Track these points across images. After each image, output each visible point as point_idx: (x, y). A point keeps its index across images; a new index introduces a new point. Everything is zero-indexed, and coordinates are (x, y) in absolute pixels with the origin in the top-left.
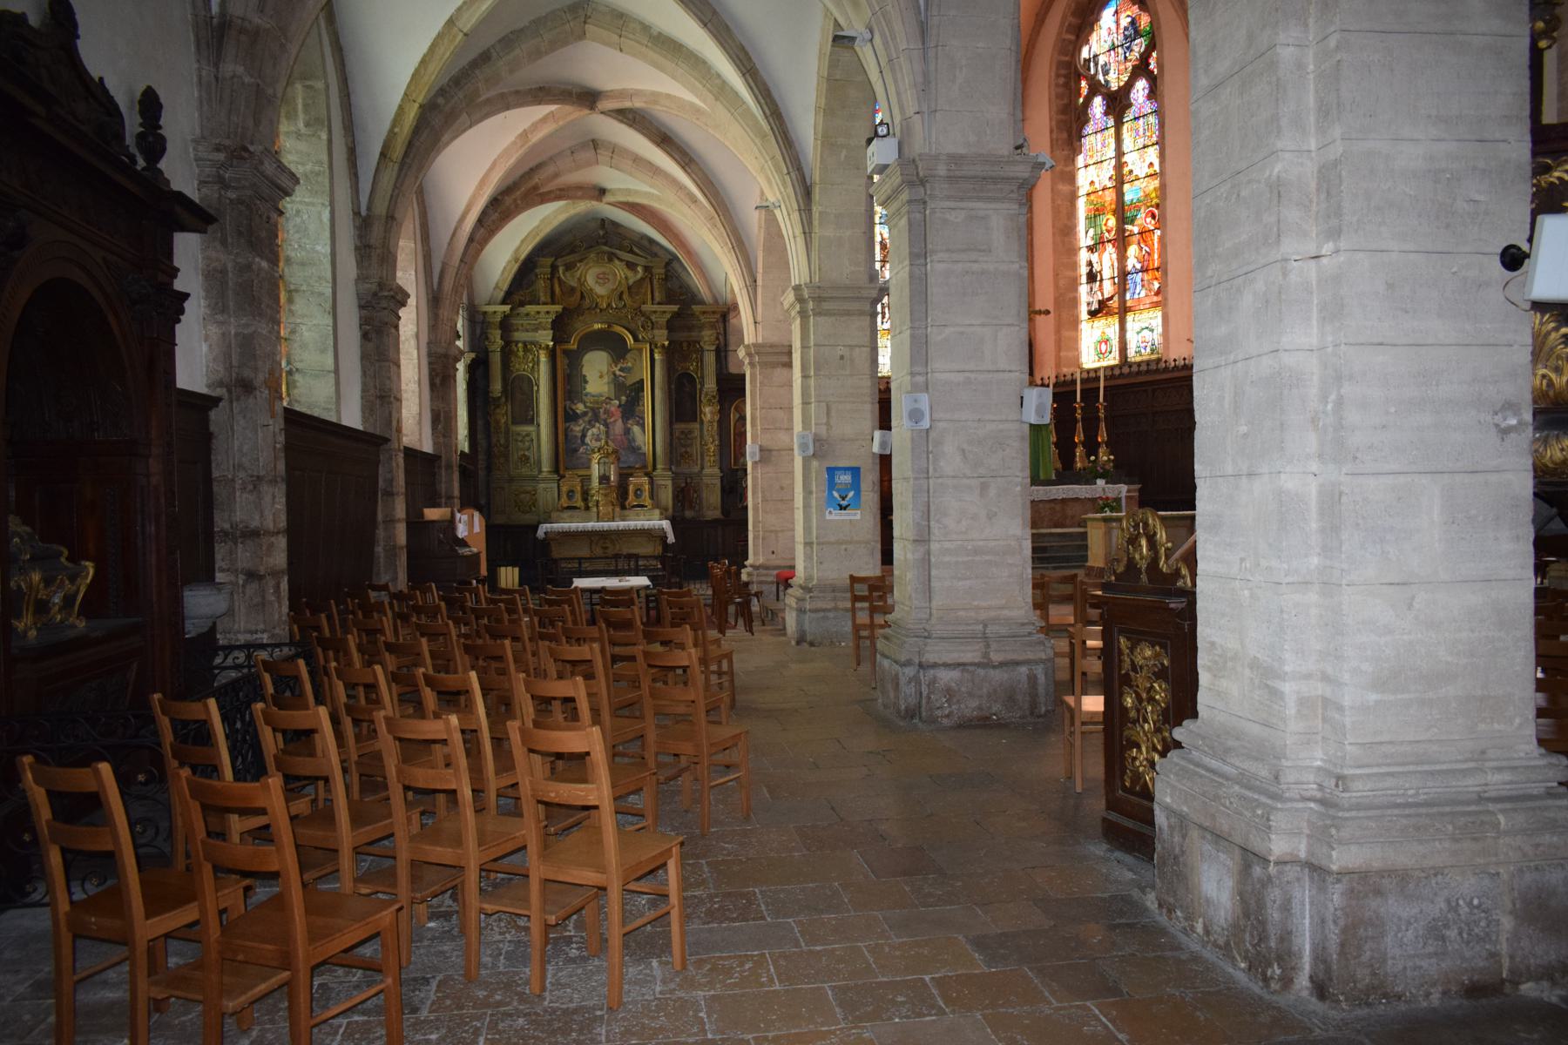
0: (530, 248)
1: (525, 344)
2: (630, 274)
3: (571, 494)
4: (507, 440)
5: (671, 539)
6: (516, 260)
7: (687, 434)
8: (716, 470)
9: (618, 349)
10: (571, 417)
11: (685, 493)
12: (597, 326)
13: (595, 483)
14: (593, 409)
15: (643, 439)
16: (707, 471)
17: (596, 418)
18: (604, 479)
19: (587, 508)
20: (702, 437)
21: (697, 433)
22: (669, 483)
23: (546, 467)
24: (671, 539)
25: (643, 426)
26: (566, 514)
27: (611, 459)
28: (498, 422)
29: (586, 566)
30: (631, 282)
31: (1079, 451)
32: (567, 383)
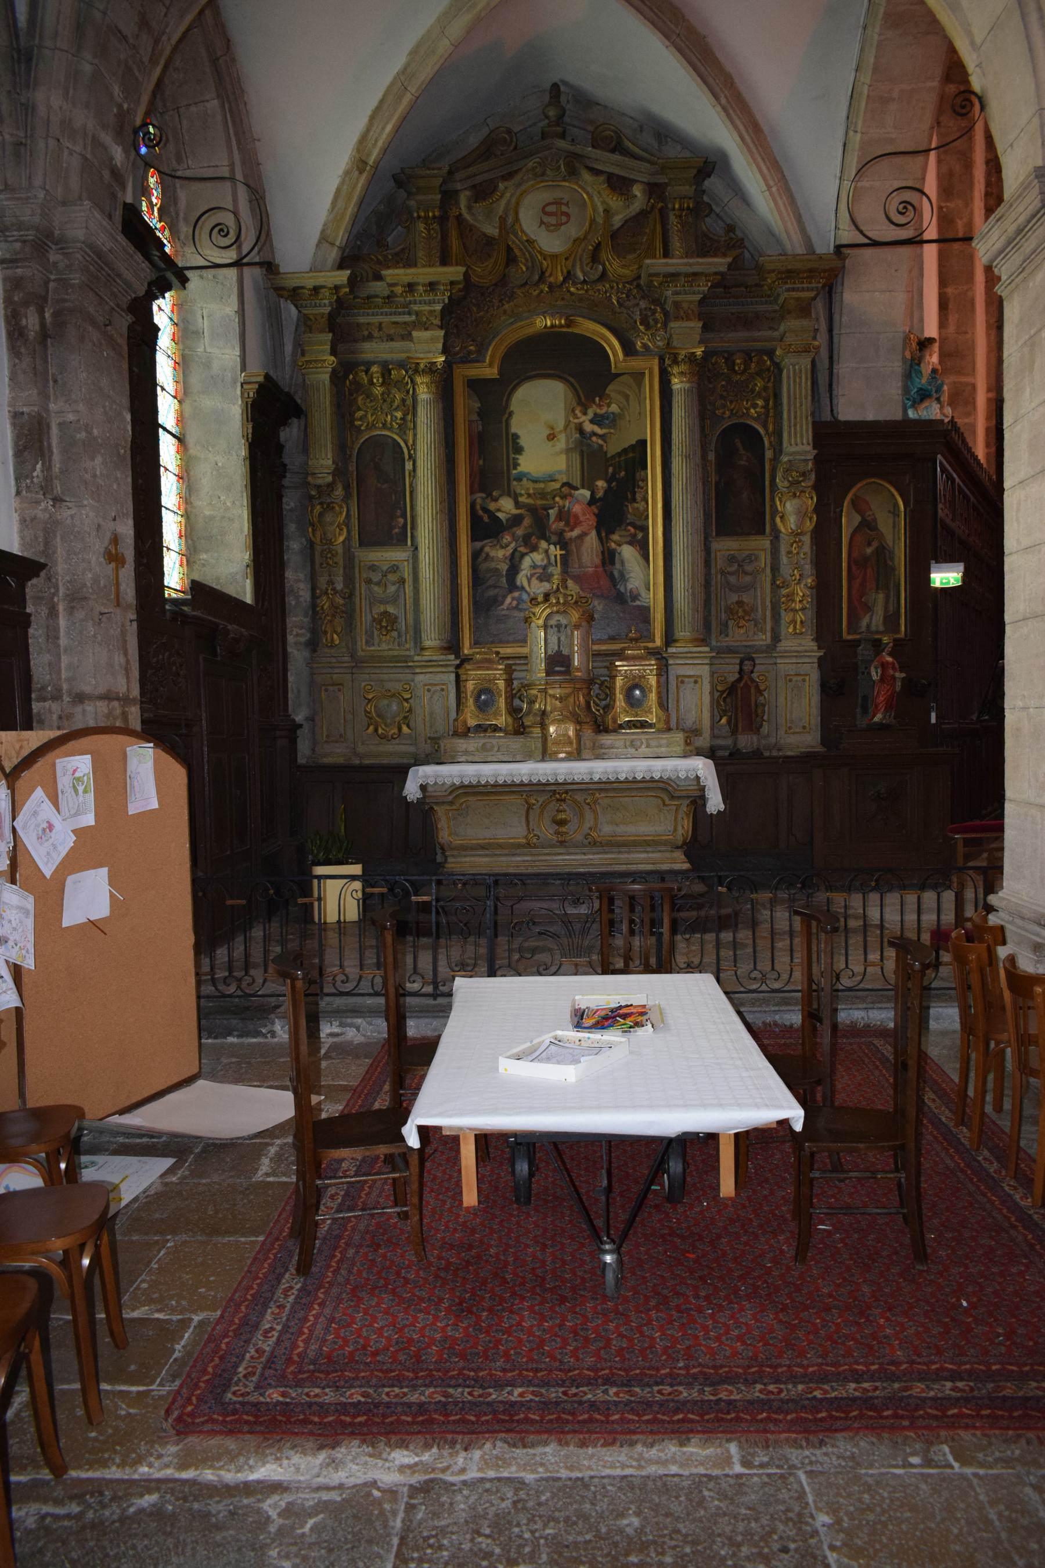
1: (386, 372)
2: (615, 202)
3: (484, 701)
4: (349, 580)
5: (715, 802)
6: (360, 164)
7: (740, 563)
8: (809, 643)
9: (586, 373)
10: (486, 527)
11: (740, 700)
12: (543, 322)
14: (532, 510)
16: (787, 644)
17: (540, 530)
20: (775, 569)
21: (764, 560)
22: (705, 671)
23: (432, 637)
24: (715, 802)
26: (471, 744)
27: (575, 616)
30: (617, 221)
32: (483, 451)
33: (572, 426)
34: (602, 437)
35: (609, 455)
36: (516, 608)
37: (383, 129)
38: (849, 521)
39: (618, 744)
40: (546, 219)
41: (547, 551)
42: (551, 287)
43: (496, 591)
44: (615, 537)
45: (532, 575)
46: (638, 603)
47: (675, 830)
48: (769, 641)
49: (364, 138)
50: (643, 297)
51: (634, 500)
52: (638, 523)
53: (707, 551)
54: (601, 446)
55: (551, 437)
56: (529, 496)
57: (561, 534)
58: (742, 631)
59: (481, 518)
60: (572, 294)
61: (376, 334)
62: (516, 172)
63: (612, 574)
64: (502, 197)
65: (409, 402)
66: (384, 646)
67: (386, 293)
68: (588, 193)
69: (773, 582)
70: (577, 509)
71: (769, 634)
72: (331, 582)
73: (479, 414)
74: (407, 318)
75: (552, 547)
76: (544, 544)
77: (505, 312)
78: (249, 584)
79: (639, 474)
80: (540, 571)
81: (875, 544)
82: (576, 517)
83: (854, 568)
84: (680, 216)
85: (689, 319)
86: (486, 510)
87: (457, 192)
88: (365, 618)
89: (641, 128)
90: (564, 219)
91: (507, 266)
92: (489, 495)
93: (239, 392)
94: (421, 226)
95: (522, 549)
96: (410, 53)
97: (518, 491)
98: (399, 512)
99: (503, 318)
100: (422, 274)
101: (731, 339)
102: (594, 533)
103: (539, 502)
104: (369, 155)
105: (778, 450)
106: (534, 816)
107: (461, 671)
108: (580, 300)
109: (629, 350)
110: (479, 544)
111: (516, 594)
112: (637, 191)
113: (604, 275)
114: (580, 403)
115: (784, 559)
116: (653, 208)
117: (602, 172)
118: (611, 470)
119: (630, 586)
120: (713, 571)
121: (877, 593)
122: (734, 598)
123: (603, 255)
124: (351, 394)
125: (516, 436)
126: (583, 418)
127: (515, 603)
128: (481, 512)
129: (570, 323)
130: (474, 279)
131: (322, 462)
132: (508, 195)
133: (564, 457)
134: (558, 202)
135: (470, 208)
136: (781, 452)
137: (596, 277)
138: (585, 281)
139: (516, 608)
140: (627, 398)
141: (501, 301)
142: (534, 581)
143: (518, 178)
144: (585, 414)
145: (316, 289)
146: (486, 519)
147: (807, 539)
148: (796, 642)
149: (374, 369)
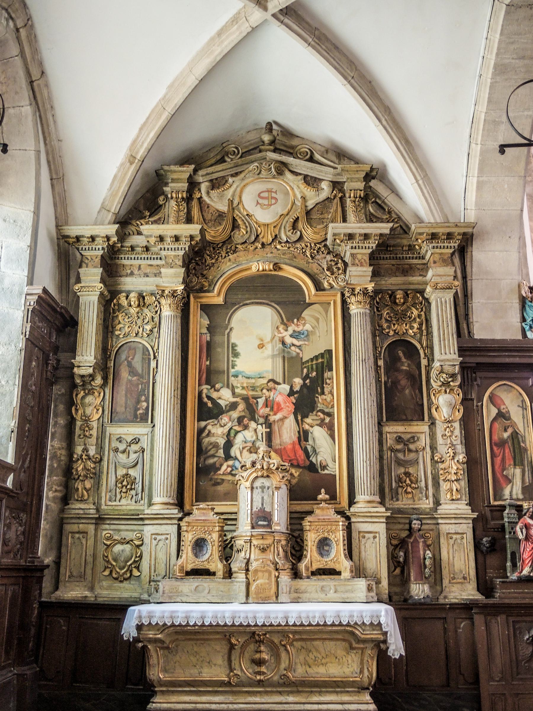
0: (152, 135)
2: (309, 192)
4: (100, 448)
5: (396, 647)
6: (132, 159)
8: (463, 507)
9: (289, 301)
10: (209, 411)
13: (244, 527)
14: (246, 399)
15: (327, 450)
16: (446, 508)
18: (262, 518)
19: (229, 574)
20: (433, 448)
21: (424, 441)
22: (381, 528)
24: (396, 647)
25: (330, 428)
28: (87, 420)
29: (48, 146)
30: (310, 204)
31: (501, 580)
32: (202, 361)
33: (277, 339)
34: (299, 347)
35: (304, 360)
36: (230, 474)
37: (148, 135)
38: (489, 412)
39: (309, 589)
40: (260, 201)
41: (255, 430)
42: (263, 245)
43: (216, 459)
44: (308, 420)
45: (243, 448)
46: (326, 472)
47: (361, 672)
48: (431, 505)
49: (134, 142)
50: (329, 253)
51: (323, 393)
52: (326, 410)
53: (380, 433)
54: (298, 354)
55: (261, 346)
56: (243, 388)
57: (266, 418)
58: (410, 496)
59: (206, 404)
60: (278, 250)
61: (136, 272)
62: (241, 172)
63: (306, 448)
64: (231, 186)
65: (156, 319)
66: (123, 502)
67: (145, 244)
68: (290, 186)
69: (432, 459)
70: (279, 399)
71: (431, 499)
72: (86, 450)
73: (208, 329)
74: (159, 262)
75: (260, 426)
76: (253, 425)
77: (230, 260)
78: (11, 447)
79: (327, 374)
80: (250, 444)
81: (510, 431)
82: (279, 404)
83: (495, 448)
84: (354, 201)
85: (362, 265)
86: (209, 398)
87: (199, 183)
88: (109, 480)
89: (327, 152)
90: (273, 201)
91: (233, 230)
92: (213, 387)
93: (23, 302)
94: (173, 203)
95: (237, 428)
96: (169, 87)
97: (235, 385)
98: (143, 398)
99: (228, 264)
100: (170, 229)
101: (392, 282)
102: (292, 417)
103: (251, 393)
104: (137, 153)
105: (431, 360)
106: (235, 655)
107: (182, 524)
108: (284, 254)
109: (319, 287)
110: (203, 424)
111: (230, 463)
112: (325, 185)
113: (301, 238)
114: (283, 323)
115: (440, 440)
116: (335, 196)
117: (300, 174)
118: (305, 370)
119: (319, 458)
120: (385, 448)
121: (515, 468)
122: (402, 470)
123: (300, 225)
124: (114, 313)
125: (234, 346)
126: (285, 333)
127: (229, 469)
128: (205, 400)
129: (277, 267)
130: (208, 238)
131: (85, 358)
132: (235, 186)
133: (270, 360)
134: (269, 191)
135: (208, 193)
136: (433, 360)
137: (296, 239)
138: (287, 242)
139: (230, 474)
140: (317, 320)
141: (227, 253)
142: (245, 453)
143: (242, 175)
144: (286, 330)
145: (93, 239)
146: (210, 405)
147: (457, 425)
148: (453, 506)
149: (132, 295)
